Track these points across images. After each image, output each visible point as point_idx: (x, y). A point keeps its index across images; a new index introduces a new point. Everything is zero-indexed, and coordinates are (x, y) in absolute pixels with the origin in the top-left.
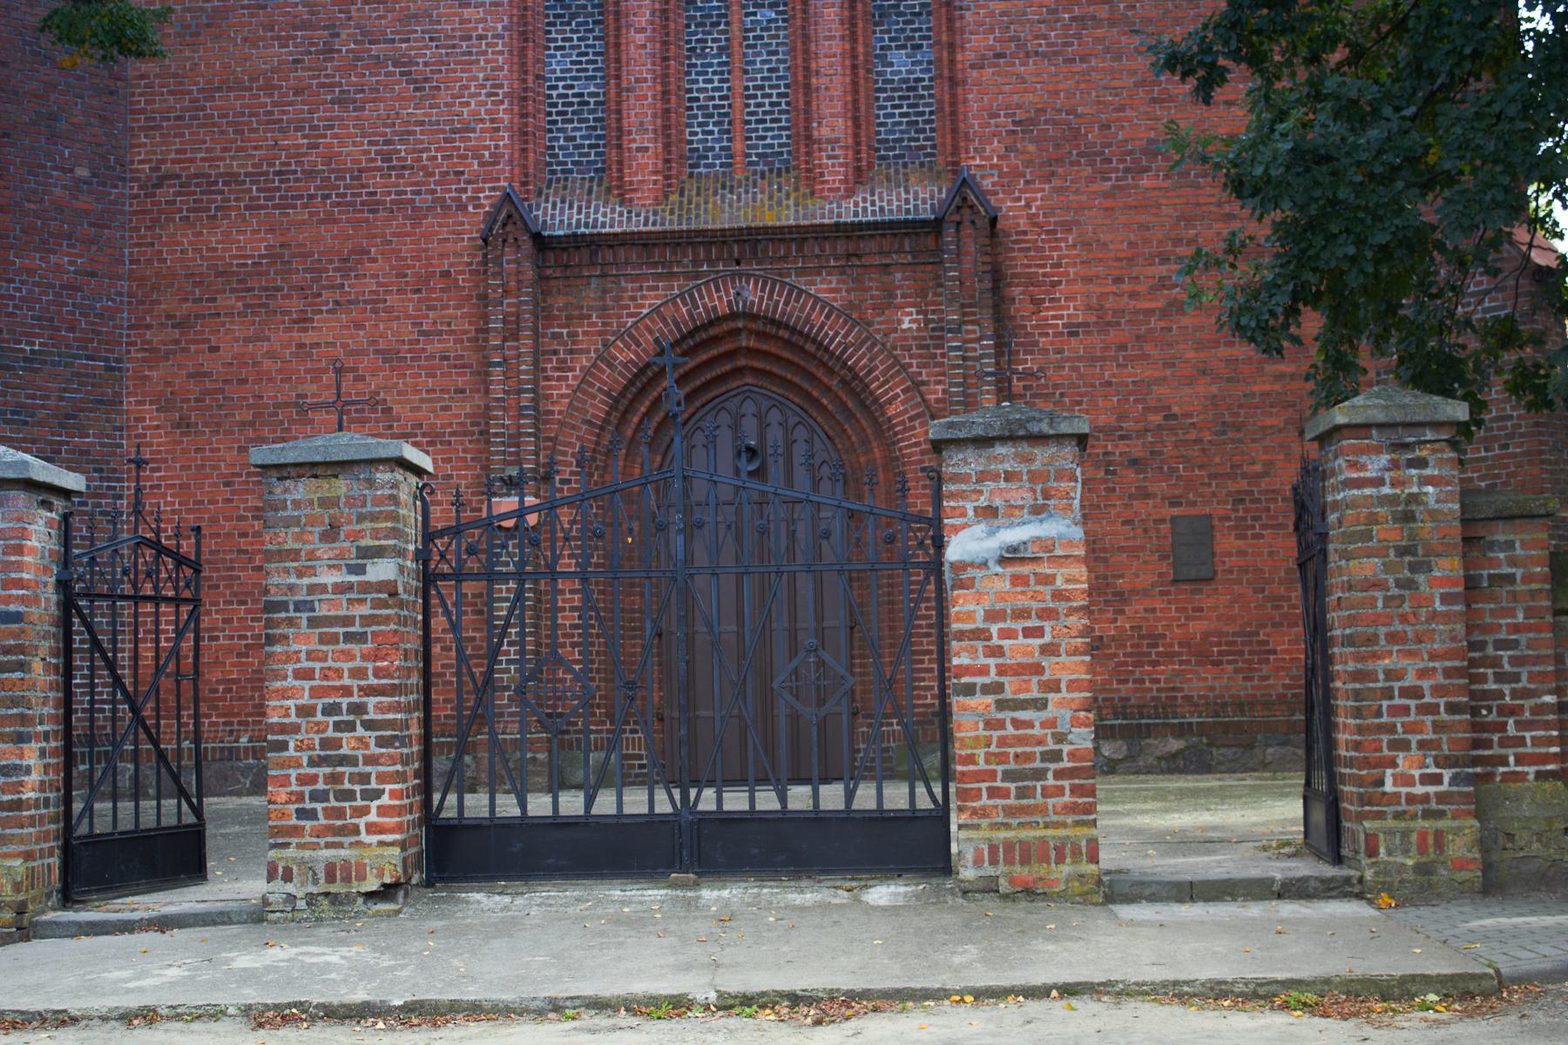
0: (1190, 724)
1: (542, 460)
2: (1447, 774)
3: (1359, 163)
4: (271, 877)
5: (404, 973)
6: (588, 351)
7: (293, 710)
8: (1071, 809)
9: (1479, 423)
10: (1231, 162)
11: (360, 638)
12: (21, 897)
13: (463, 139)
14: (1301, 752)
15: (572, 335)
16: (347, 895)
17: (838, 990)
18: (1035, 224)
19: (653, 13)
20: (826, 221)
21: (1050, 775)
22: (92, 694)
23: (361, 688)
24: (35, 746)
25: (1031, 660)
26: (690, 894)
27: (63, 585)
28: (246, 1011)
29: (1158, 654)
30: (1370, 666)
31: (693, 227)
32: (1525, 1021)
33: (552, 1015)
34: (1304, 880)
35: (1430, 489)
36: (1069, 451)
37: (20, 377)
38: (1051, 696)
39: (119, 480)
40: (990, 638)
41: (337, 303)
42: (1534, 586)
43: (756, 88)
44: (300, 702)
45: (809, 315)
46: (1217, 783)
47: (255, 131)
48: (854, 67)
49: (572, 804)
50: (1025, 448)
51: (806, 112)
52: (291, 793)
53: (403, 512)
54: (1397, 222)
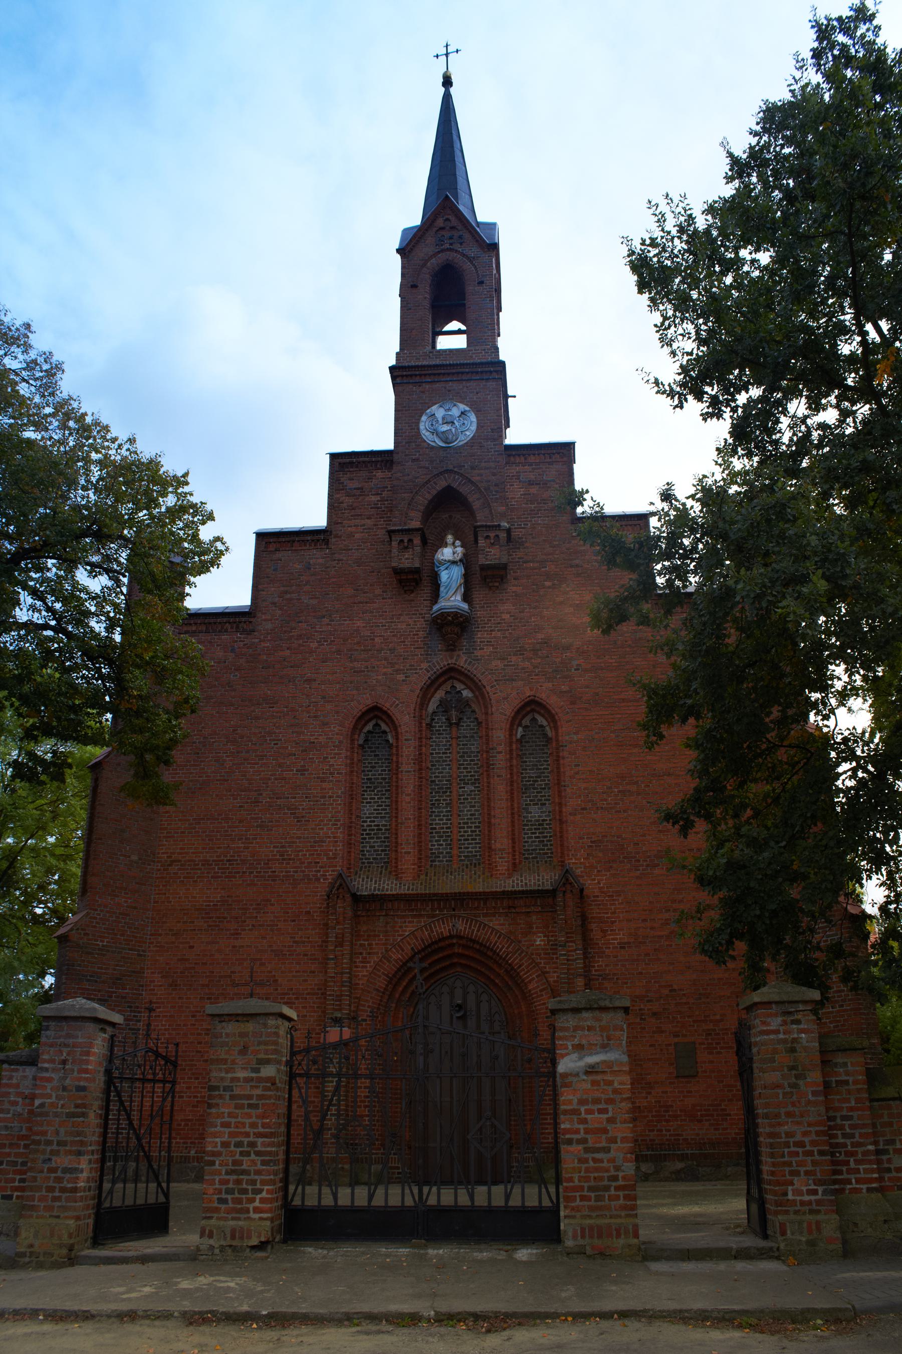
0: (687, 1154)
1: (352, 1009)
2: (820, 1189)
3: (759, 869)
4: (202, 1236)
5: (269, 1295)
6: (378, 953)
7: (219, 1144)
8: (624, 1208)
9: (827, 999)
10: (697, 868)
11: (255, 1106)
12: (71, 1241)
13: (319, 846)
14: (745, 1169)
15: (369, 945)
16: (241, 1247)
17: (499, 1312)
18: (602, 892)
19: (414, 787)
20: (498, 890)
21: (612, 1189)
22: (118, 1124)
23: (254, 1133)
24: (87, 1157)
25: (602, 1126)
26: (422, 1252)
27: (108, 1072)
28: (184, 1314)
29: (669, 1116)
30: (777, 1130)
31: (432, 892)
32: (870, 1339)
33: (346, 1323)
34: (748, 1249)
35: (803, 1035)
36: (620, 1015)
37: (95, 958)
38: (612, 1145)
39: (139, 1012)
40: (580, 1114)
41: (253, 925)
42: (859, 1086)
43: (464, 823)
44: (223, 1139)
45: (489, 937)
46: (701, 1188)
47: (219, 839)
48: (513, 814)
49: (361, 1196)
50: (597, 1013)
51: (489, 835)
52: (215, 1189)
53: (280, 1041)
54: (780, 898)
